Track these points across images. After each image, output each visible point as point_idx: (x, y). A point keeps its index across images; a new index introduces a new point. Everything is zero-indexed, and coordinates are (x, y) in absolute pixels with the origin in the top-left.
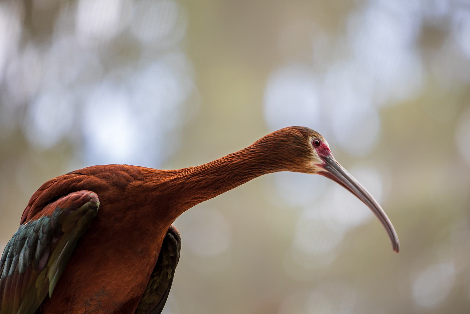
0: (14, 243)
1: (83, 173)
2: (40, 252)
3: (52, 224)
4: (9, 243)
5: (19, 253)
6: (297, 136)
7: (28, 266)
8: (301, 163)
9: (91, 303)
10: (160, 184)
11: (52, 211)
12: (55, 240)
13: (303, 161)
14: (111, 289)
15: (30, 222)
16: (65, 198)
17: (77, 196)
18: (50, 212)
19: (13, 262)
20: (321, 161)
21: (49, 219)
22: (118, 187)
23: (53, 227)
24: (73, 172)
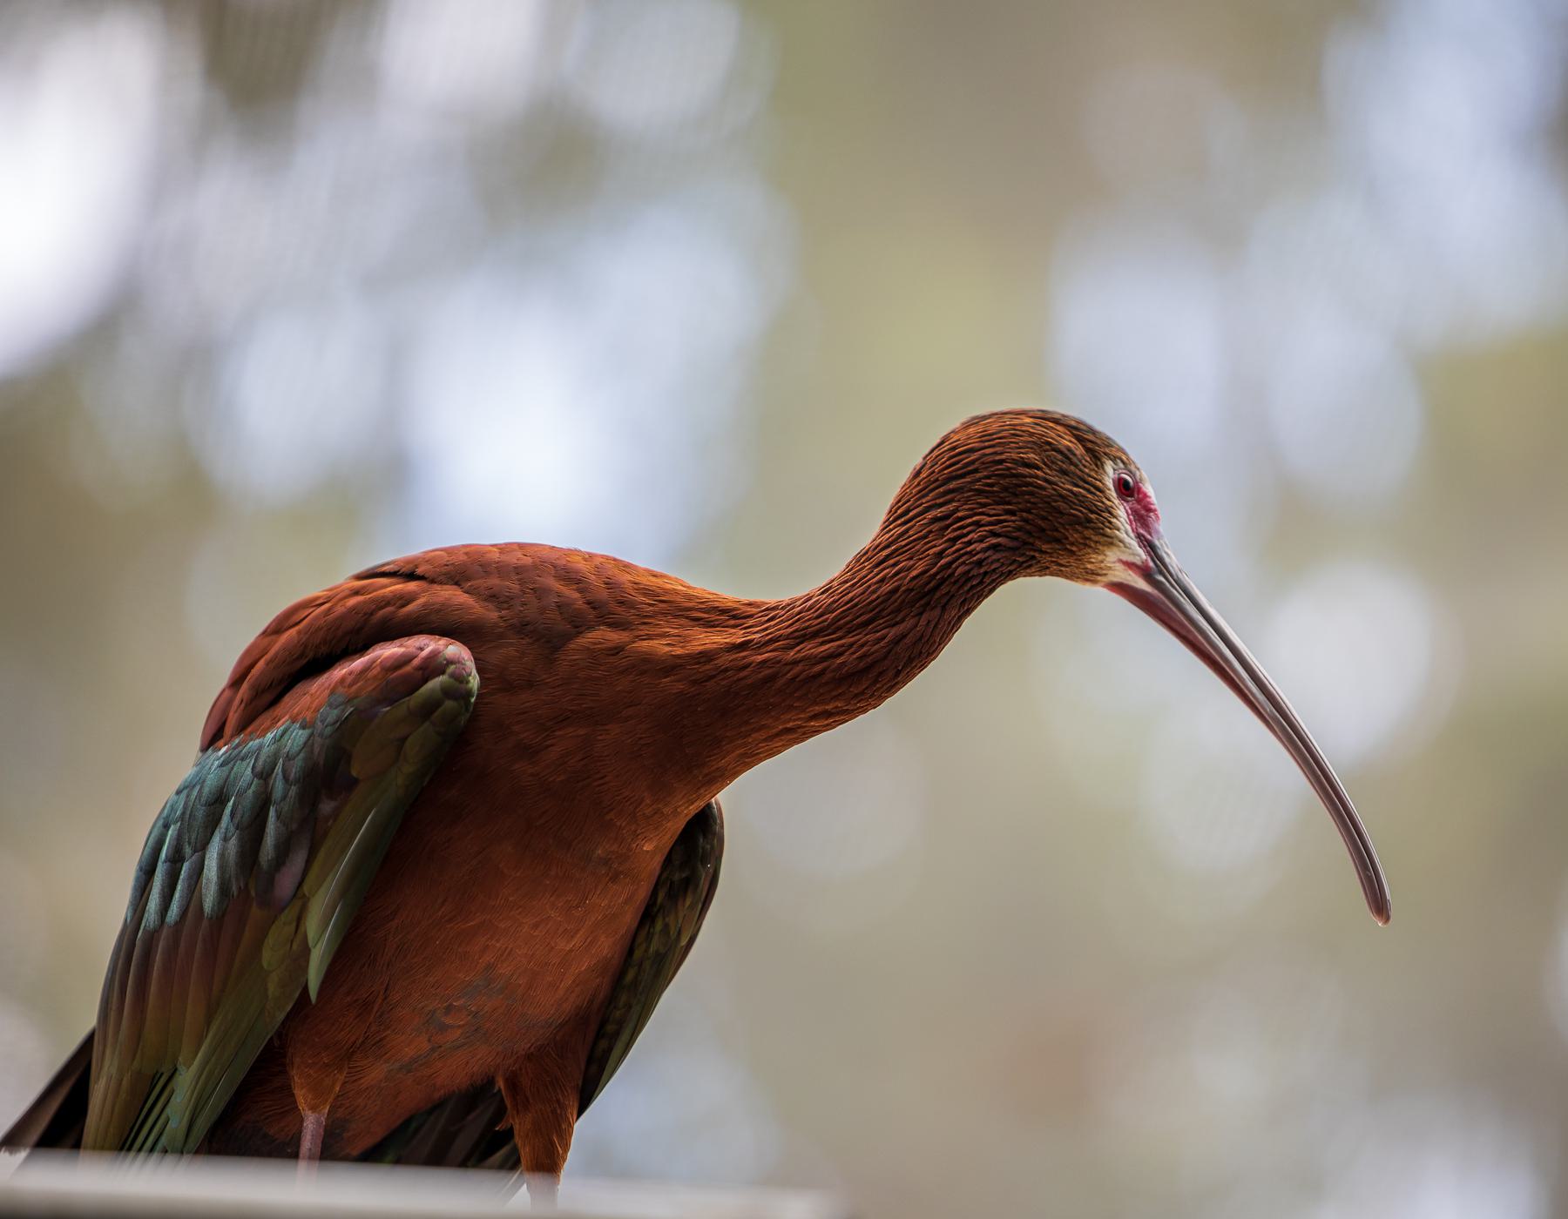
0: (183, 813)
1: (419, 571)
2: (277, 847)
3: (316, 750)
4: (166, 811)
5: (202, 847)
6: (1069, 449)
7: (235, 894)
8: (1080, 550)
9: (448, 1021)
10: (688, 655)
11: (314, 706)
12: (326, 807)
13: (1088, 542)
14: (512, 975)
15: (237, 741)
16: (359, 663)
17: (402, 655)
18: (309, 708)
19: (181, 877)
20: (1141, 555)
21: (306, 733)
22: (537, 640)
23: (322, 762)
24: (383, 565)
